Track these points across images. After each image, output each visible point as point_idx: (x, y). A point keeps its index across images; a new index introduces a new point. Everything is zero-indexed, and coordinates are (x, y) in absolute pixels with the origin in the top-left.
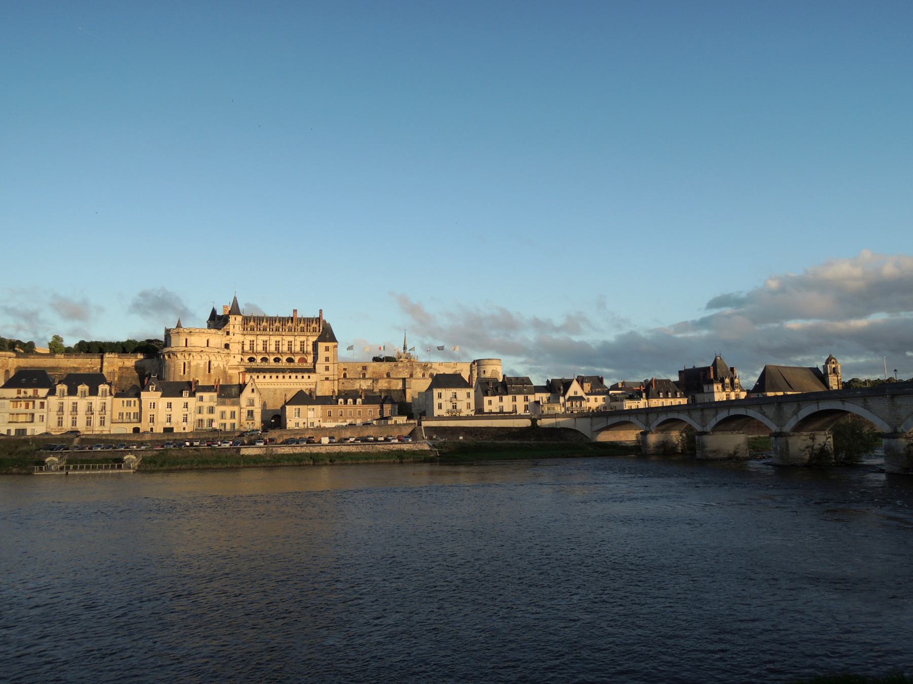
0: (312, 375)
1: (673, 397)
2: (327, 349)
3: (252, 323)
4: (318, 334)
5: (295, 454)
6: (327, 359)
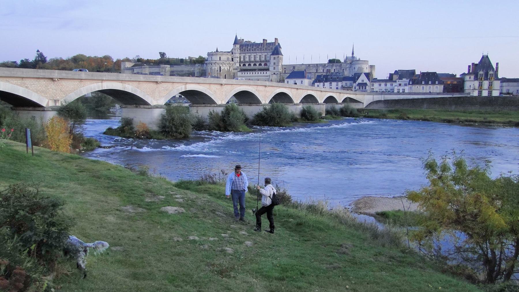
0: (268, 72)
2: (274, 58)
5: (93, 119)
6: (274, 63)
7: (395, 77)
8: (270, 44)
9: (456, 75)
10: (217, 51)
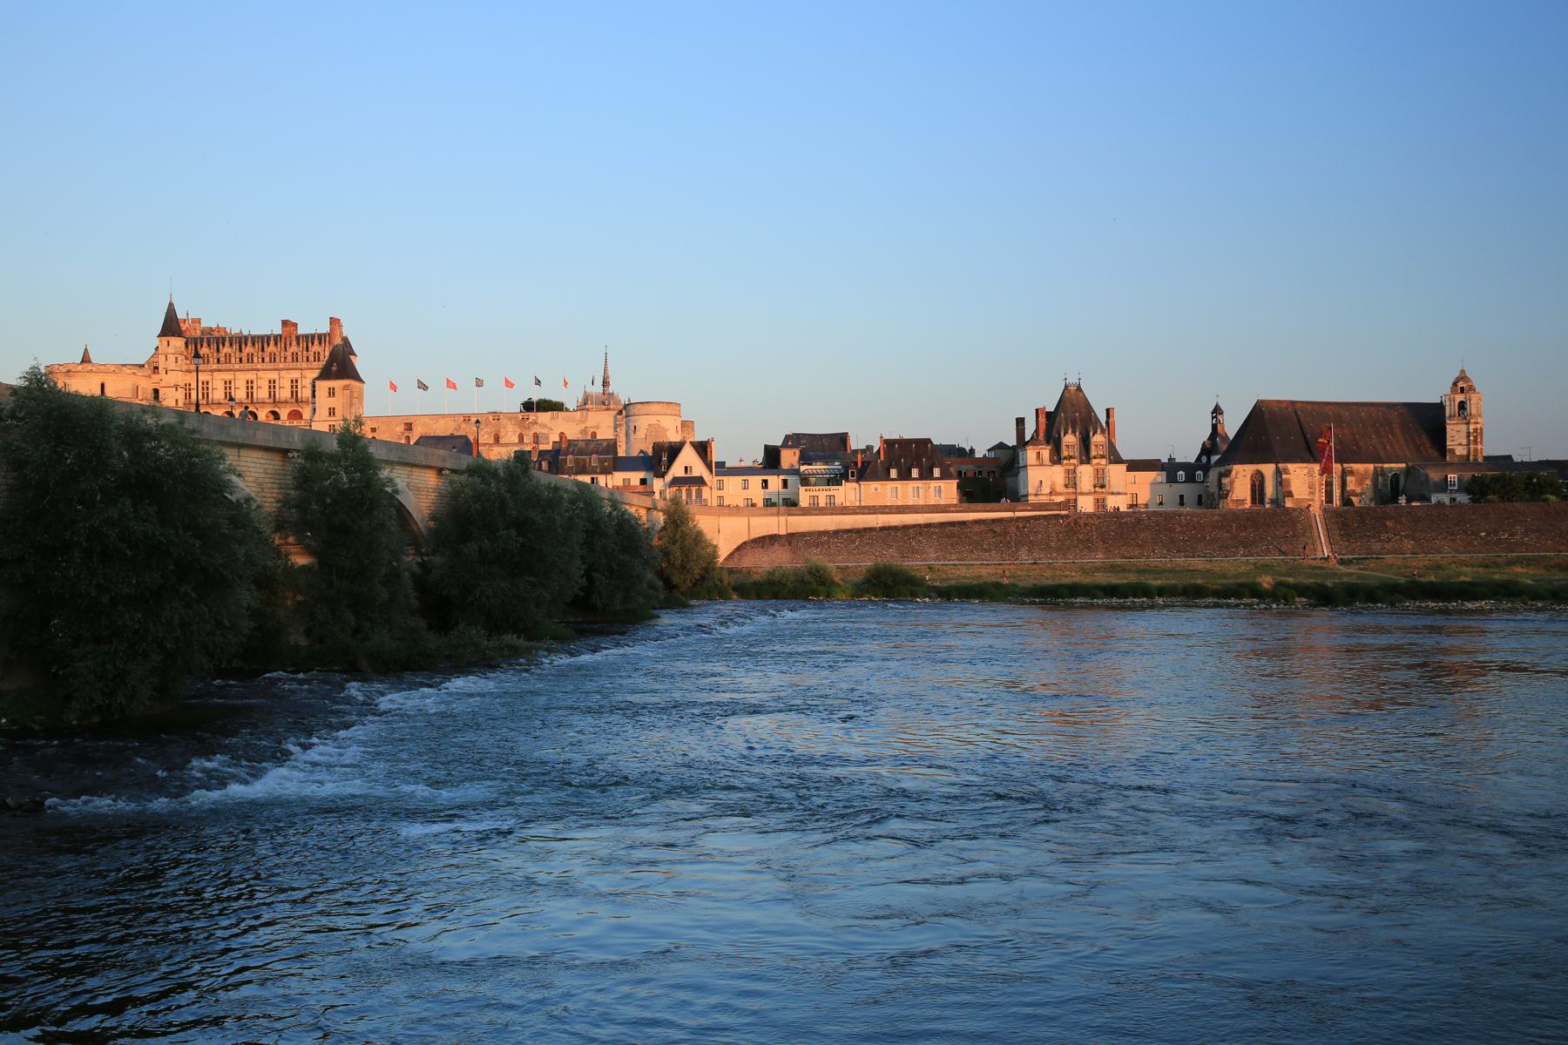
1: (921, 477)
2: (332, 393)
3: (272, 348)
4: (322, 364)
7: (789, 458)
8: (309, 339)
9: (972, 451)
10: (86, 359)
